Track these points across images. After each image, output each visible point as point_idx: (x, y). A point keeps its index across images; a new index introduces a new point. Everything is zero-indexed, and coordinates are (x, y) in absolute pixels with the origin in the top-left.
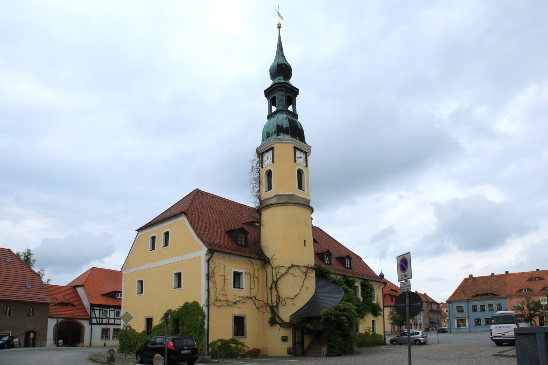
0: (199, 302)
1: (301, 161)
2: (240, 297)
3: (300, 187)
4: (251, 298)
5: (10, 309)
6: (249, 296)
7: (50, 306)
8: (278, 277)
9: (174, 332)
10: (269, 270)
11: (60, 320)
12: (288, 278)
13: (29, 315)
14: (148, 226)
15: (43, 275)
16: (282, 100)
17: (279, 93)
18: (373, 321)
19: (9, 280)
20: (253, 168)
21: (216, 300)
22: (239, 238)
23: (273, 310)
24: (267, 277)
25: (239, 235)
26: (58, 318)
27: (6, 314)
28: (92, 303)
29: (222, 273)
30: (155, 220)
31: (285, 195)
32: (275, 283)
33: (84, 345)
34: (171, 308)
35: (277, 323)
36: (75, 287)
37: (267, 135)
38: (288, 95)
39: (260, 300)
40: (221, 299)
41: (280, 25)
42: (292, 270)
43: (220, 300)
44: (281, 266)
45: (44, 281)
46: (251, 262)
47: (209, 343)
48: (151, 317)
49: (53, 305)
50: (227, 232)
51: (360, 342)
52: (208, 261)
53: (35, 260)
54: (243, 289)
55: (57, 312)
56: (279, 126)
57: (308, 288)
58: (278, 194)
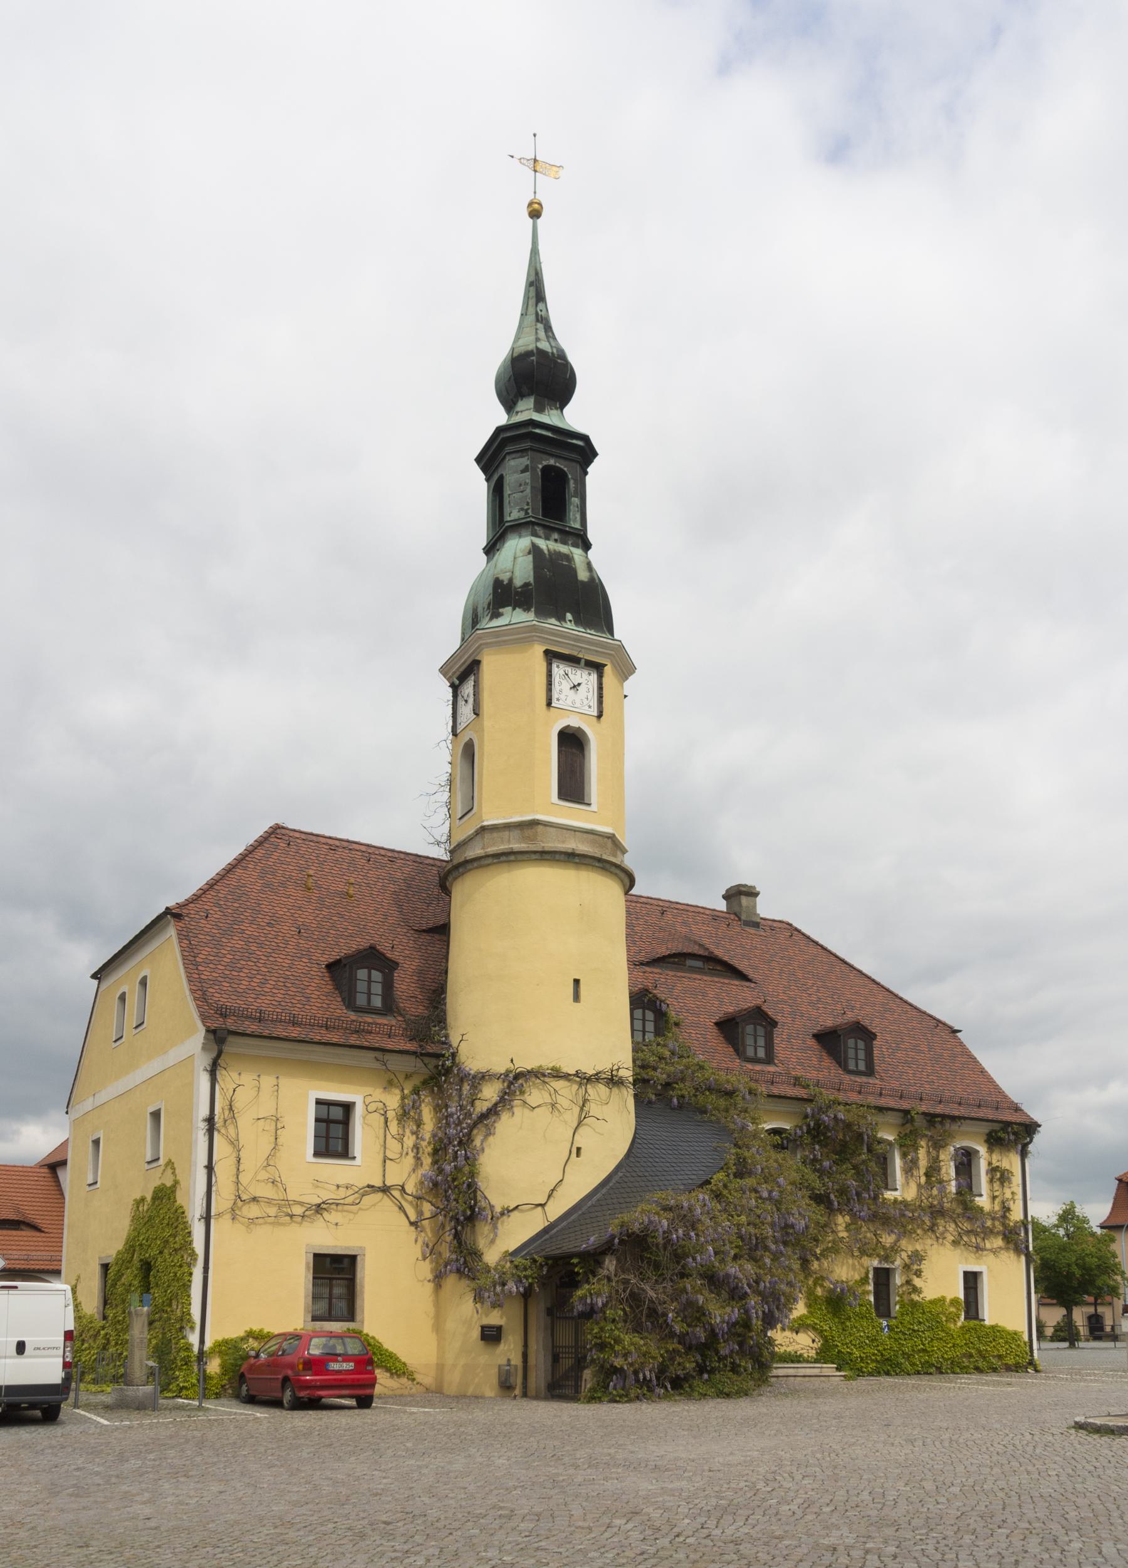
4: (385, 1190)
6: (378, 1183)
21: (240, 1203)
22: (361, 986)
25: (362, 974)
29: (266, 1108)
37: (473, 619)
38: (545, 463)
41: (536, 206)
43: (254, 1199)
56: (503, 581)
58: (485, 823)
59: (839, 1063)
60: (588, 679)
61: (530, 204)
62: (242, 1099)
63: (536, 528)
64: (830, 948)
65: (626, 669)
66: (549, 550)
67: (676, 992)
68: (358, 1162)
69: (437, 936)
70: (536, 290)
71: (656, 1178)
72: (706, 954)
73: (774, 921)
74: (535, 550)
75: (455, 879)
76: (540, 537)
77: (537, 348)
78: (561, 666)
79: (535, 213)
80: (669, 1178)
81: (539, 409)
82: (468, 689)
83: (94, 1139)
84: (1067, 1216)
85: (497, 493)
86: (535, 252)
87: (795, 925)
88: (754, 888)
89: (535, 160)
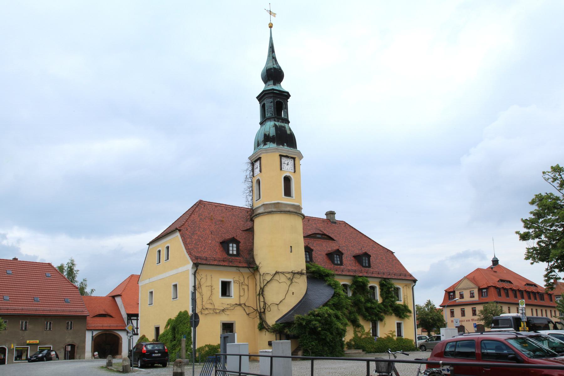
0: (188, 312)
1: (288, 166)
2: (228, 304)
3: (288, 192)
4: (240, 305)
5: (50, 323)
6: (238, 303)
7: (87, 318)
8: (265, 284)
9: (173, 340)
10: (258, 277)
11: (95, 333)
12: (274, 285)
13: (68, 329)
14: (155, 241)
15: (85, 285)
16: (270, 107)
17: (268, 100)
18: (399, 325)
19: (49, 295)
20: (246, 177)
22: (231, 248)
23: (261, 315)
24: (256, 284)
26: (93, 331)
27: (47, 329)
28: (129, 313)
29: (209, 283)
30: (164, 233)
31: (271, 204)
32: (262, 290)
33: (122, 356)
34: (171, 318)
35: (264, 328)
36: (114, 297)
37: (258, 144)
38: (277, 100)
39: (250, 307)
40: (208, 307)
41: (271, 25)
42: (277, 277)
43: (207, 309)
44: (267, 273)
45: (88, 292)
46: (239, 270)
47: (196, 349)
48: (158, 327)
49: (91, 317)
50: (221, 243)
51: (378, 348)
52: (195, 274)
53: (78, 271)
54: (232, 296)
55: (94, 324)
56: (267, 135)
57: (294, 294)
58: (265, 203)
59: (361, 264)
60: (291, 162)
61: (269, 24)
62: (203, 281)
63: (275, 119)
64: (356, 229)
65: (301, 157)
66: (279, 125)
67: (314, 245)
68: (233, 298)
69: (248, 232)
70: (272, 49)
71: (319, 301)
72: (322, 233)
73: (340, 221)
74: (275, 126)
75: (256, 218)
76: (276, 121)
77: (273, 67)
78: (284, 159)
79: (271, 27)
80: (317, 300)
81: (274, 84)
82: (257, 164)
83: (150, 291)
84: (429, 303)
85: (263, 107)
86: (271, 38)
87: (346, 222)
88: (334, 212)
89: (270, 11)
